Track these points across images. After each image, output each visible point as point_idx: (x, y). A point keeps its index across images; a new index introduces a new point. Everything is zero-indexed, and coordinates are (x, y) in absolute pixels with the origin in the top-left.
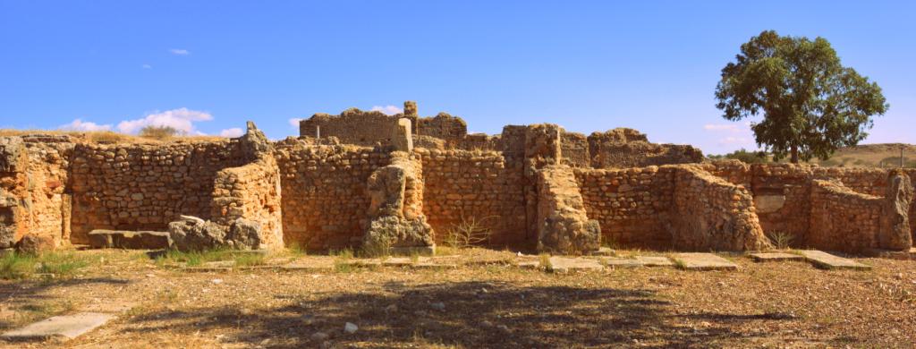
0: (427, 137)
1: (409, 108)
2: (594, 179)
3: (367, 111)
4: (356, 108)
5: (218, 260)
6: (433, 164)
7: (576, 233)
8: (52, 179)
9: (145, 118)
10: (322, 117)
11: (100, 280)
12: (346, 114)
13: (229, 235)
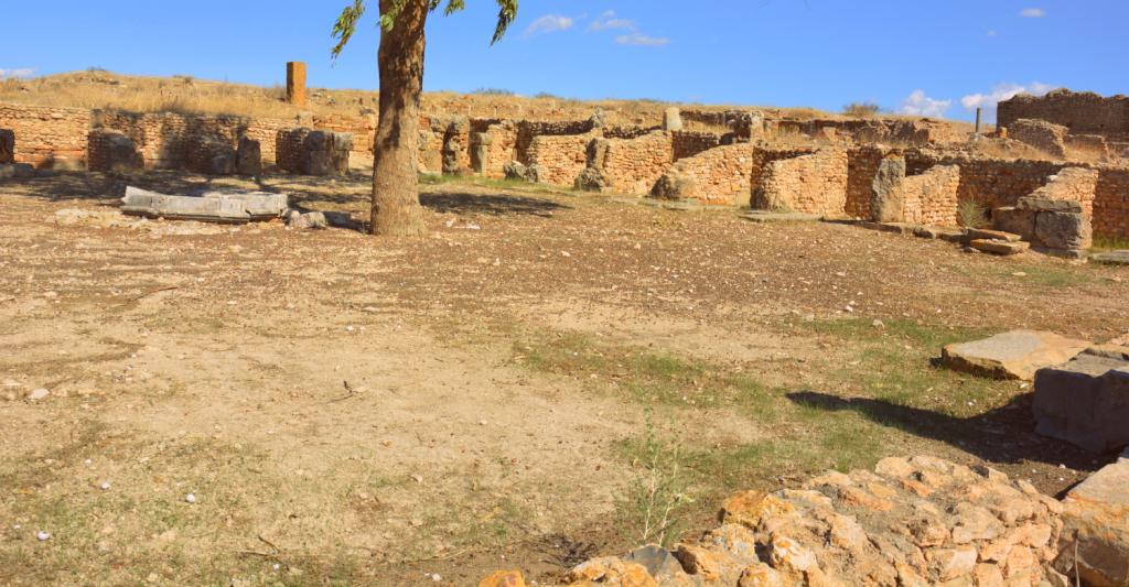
0: (1043, 123)
3: (1077, 91)
4: (1066, 88)
10: (1023, 98)
11: (1079, 165)
12: (1052, 95)
13: (527, 173)
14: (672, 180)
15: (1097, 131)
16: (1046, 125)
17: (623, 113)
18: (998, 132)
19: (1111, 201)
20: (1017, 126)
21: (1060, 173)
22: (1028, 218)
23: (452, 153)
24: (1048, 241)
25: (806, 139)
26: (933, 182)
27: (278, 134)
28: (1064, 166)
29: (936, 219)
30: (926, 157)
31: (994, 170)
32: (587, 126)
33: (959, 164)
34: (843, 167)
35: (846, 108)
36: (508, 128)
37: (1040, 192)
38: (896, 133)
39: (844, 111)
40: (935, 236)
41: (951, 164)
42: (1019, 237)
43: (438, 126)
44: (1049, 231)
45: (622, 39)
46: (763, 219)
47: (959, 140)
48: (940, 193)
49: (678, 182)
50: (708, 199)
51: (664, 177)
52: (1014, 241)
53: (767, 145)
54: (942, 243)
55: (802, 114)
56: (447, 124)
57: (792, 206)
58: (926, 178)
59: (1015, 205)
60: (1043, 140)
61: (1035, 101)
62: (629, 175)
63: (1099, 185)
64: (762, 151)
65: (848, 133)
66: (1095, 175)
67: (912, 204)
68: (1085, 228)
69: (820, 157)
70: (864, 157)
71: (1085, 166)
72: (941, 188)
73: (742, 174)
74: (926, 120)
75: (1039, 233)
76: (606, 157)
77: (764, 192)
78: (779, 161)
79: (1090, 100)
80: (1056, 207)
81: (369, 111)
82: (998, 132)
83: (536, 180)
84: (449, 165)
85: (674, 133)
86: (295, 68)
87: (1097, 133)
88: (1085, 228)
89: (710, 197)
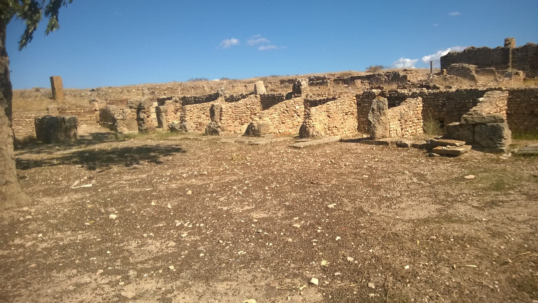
0: (464, 65)
1: (507, 42)
2: (314, 103)
5: (39, 152)
6: (264, 99)
7: (253, 128)
8: (177, 108)
9: (436, 54)
10: (453, 54)
11: (495, 89)
14: (256, 125)
15: (490, 66)
16: (466, 65)
18: (442, 72)
19: (517, 109)
20: (451, 68)
21: (485, 95)
22: (469, 129)
23: (142, 120)
24: (483, 143)
25: (346, 87)
26: (407, 110)
27: (35, 121)
28: (487, 91)
29: (410, 131)
30: (402, 94)
32: (215, 97)
33: (421, 97)
34: (354, 105)
35: (368, 69)
36: (176, 102)
37: (474, 111)
38: (390, 79)
39: (366, 70)
40: (409, 146)
41: (417, 97)
42: (464, 143)
43: (132, 105)
44: (484, 137)
45: (261, 48)
46: (302, 147)
47: (423, 79)
48: (411, 115)
49: (259, 125)
50: (279, 132)
51: (251, 123)
52: (461, 146)
53: (311, 97)
54: (415, 151)
55: (346, 74)
56: (138, 104)
57: (323, 134)
58: (402, 108)
59: (459, 120)
60: (466, 74)
61: (459, 54)
62: (236, 123)
63: (509, 100)
64: (309, 101)
65: (367, 81)
66: (506, 94)
67: (394, 125)
68: (507, 132)
69: (338, 102)
70: (366, 98)
71: (500, 89)
72: (412, 112)
73: (298, 115)
74: (405, 70)
75: (477, 138)
76: (221, 114)
77: (306, 127)
78: (313, 108)
79: (485, 51)
81: (94, 100)
82: (442, 72)
83: (186, 131)
84: (141, 126)
85: (261, 95)
86: (54, 79)
87: (490, 67)
88: (507, 132)
89: (281, 131)
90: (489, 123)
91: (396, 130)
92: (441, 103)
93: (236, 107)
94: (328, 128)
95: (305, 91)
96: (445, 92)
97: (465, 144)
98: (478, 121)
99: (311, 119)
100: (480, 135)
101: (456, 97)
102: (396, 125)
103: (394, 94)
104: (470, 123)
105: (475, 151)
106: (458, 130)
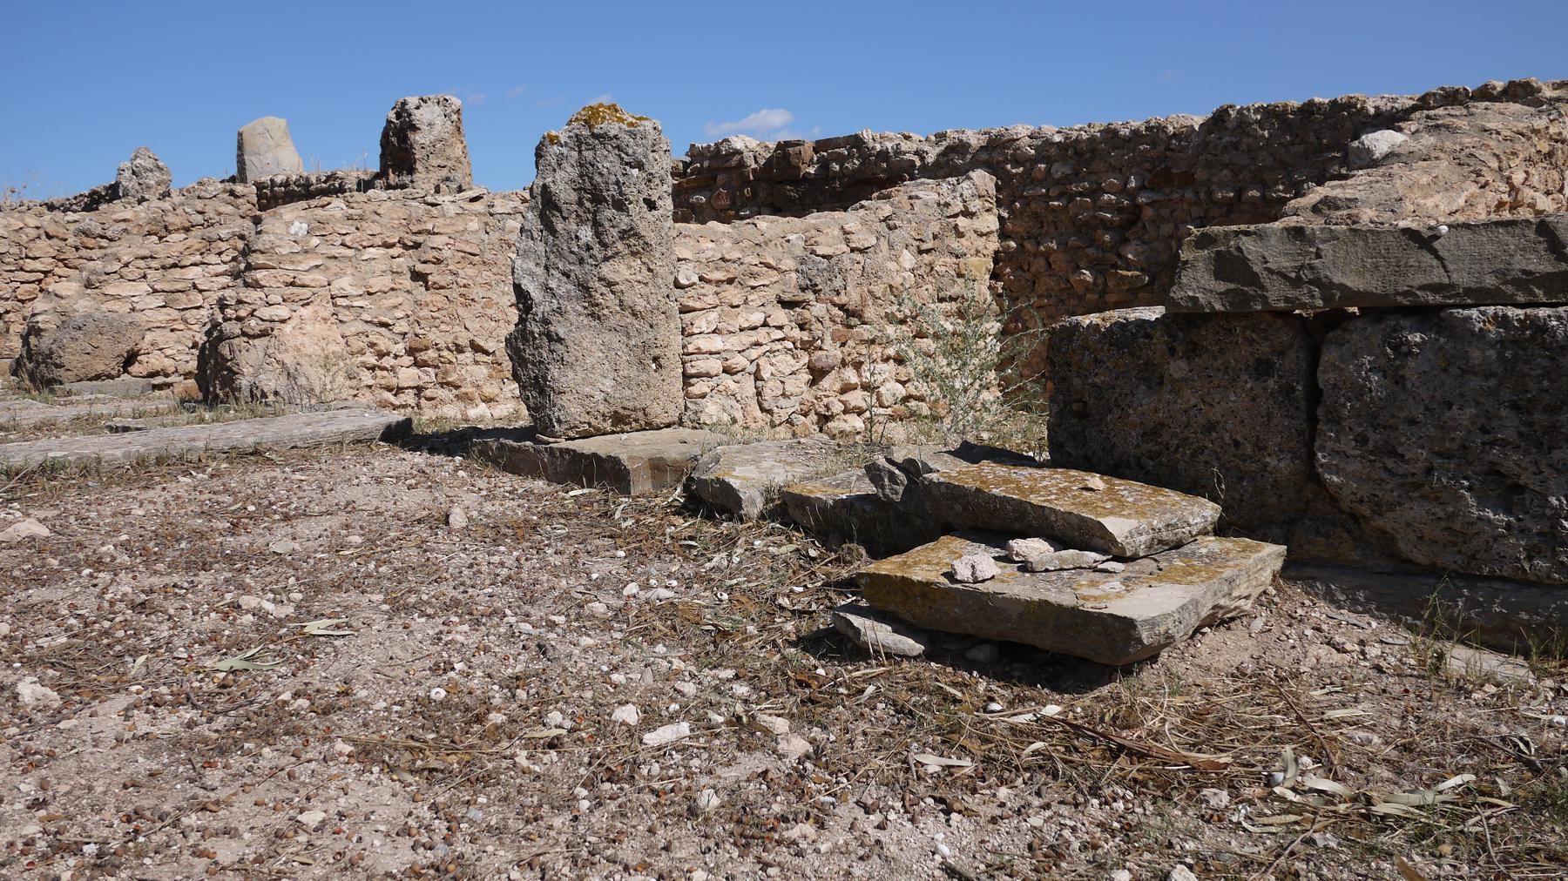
17: (1000, 295)
22: (1262, 368)
29: (892, 390)
31: (1122, 171)
33: (993, 168)
37: (1328, 203)
40: (754, 504)
41: (962, 172)
42: (1205, 511)
72: (908, 259)
80: (1462, 278)
90: (1481, 296)
91: (757, 377)
92: (1109, 207)
93: (86, 233)
94: (411, 351)
95: (434, 161)
96: (1135, 132)
97: (1220, 530)
98: (1354, 282)
99: (257, 285)
100: (1374, 437)
101: (1208, 165)
102: (761, 335)
103: (841, 159)
104: (1276, 293)
105: (1321, 611)
106: (1152, 377)
